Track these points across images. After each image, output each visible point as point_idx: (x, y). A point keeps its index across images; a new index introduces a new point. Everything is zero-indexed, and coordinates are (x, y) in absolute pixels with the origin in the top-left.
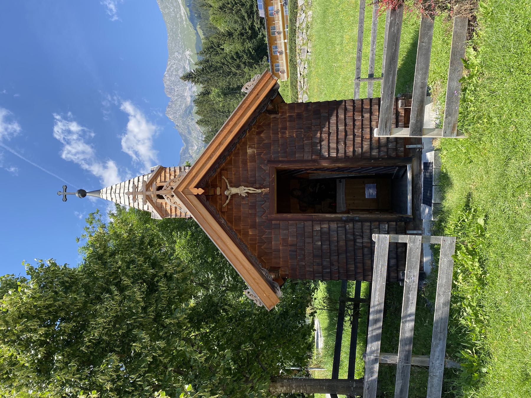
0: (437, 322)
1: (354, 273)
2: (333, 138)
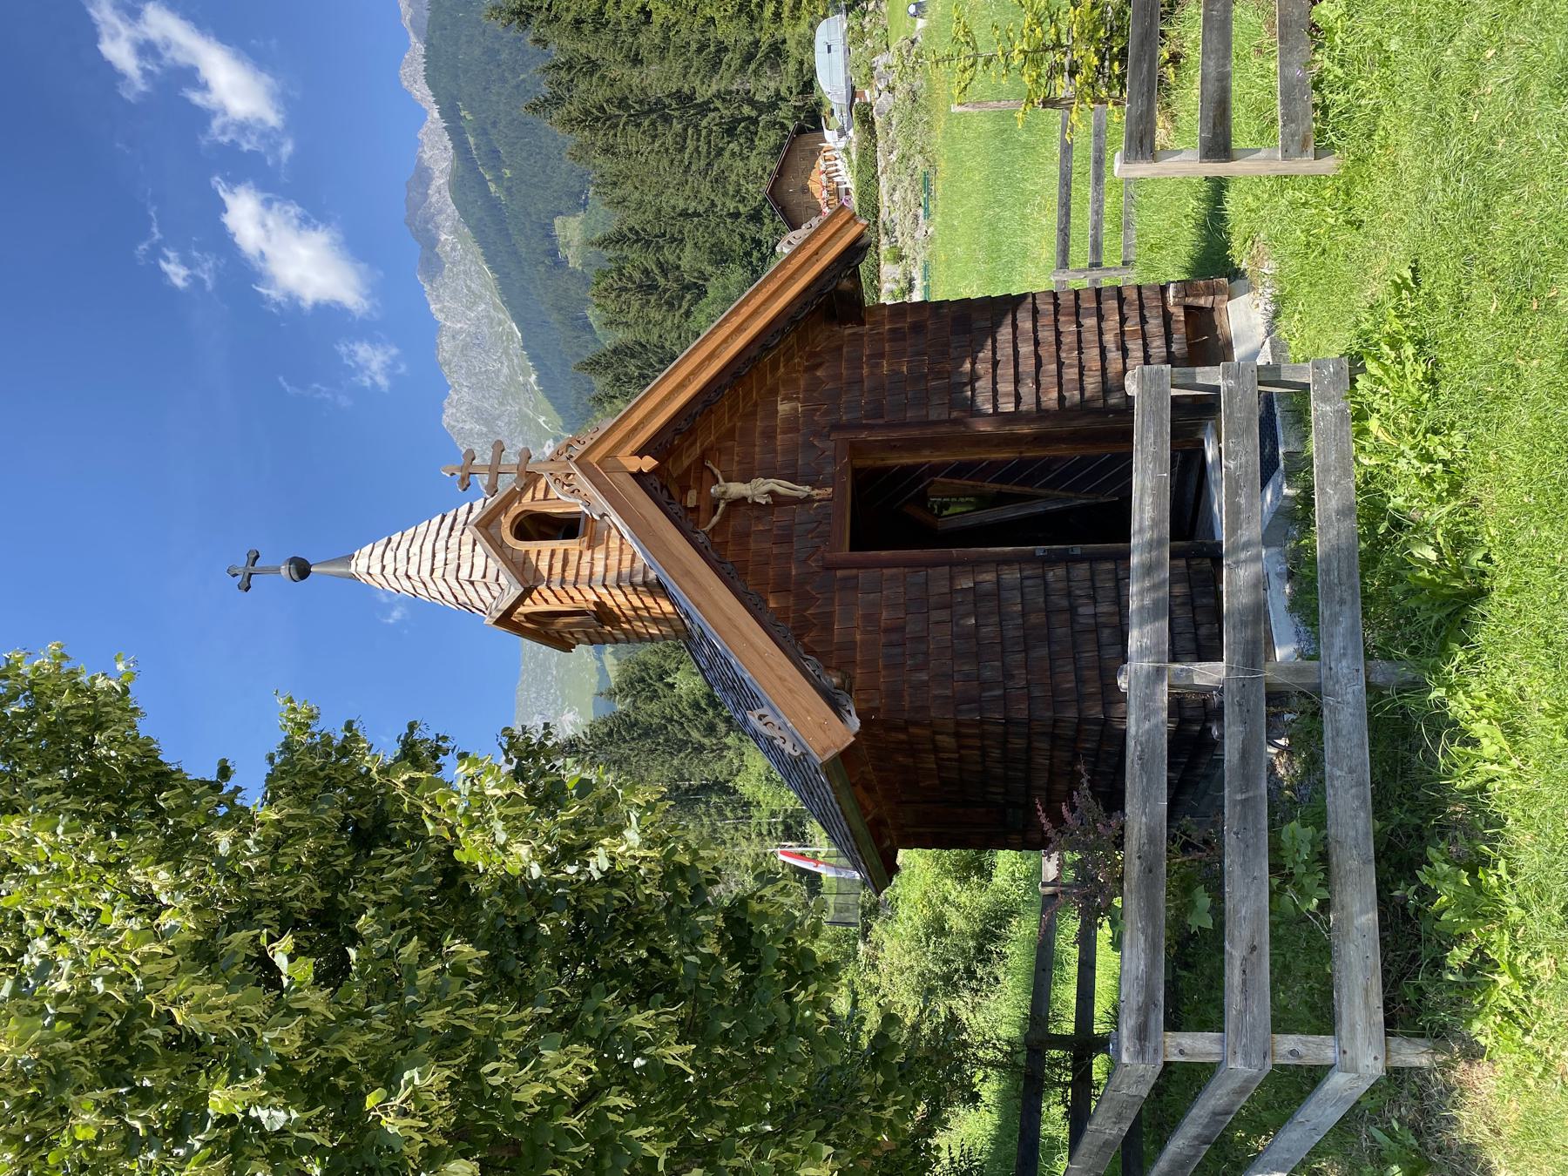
0: (1327, 558)
2: (1006, 371)
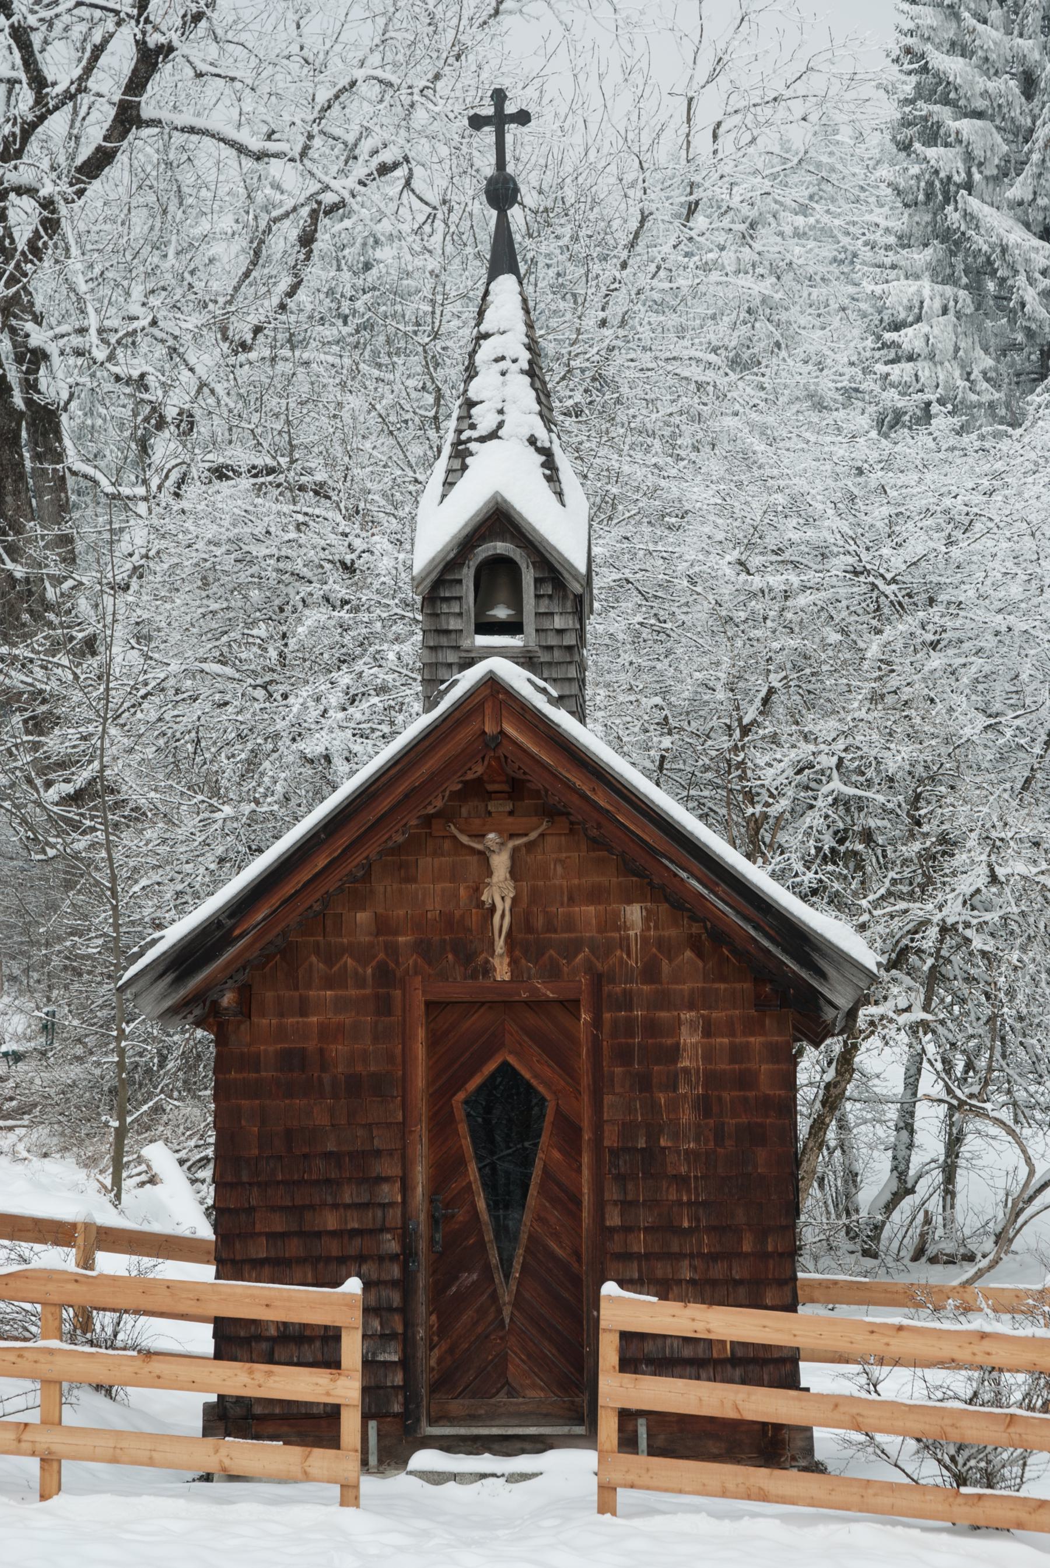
1: (238, 1257)
